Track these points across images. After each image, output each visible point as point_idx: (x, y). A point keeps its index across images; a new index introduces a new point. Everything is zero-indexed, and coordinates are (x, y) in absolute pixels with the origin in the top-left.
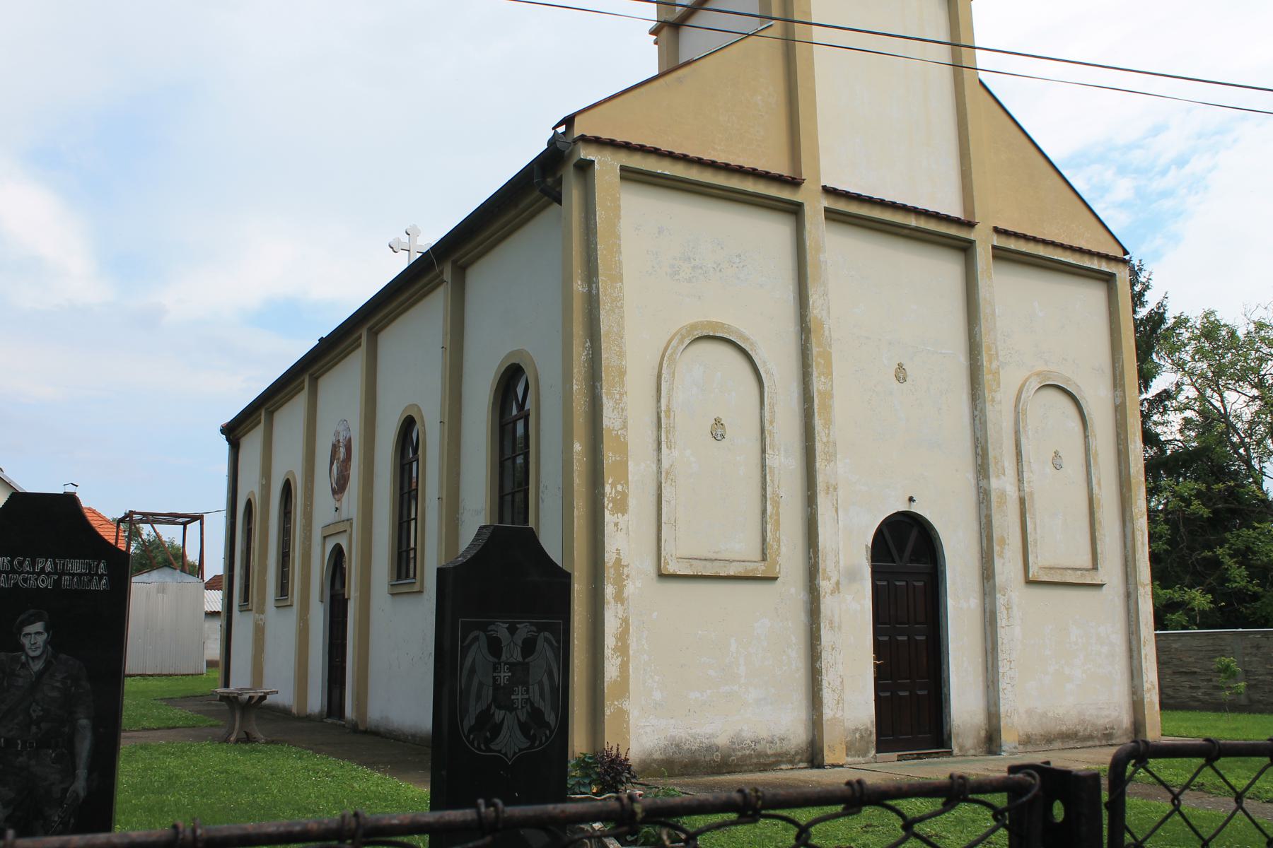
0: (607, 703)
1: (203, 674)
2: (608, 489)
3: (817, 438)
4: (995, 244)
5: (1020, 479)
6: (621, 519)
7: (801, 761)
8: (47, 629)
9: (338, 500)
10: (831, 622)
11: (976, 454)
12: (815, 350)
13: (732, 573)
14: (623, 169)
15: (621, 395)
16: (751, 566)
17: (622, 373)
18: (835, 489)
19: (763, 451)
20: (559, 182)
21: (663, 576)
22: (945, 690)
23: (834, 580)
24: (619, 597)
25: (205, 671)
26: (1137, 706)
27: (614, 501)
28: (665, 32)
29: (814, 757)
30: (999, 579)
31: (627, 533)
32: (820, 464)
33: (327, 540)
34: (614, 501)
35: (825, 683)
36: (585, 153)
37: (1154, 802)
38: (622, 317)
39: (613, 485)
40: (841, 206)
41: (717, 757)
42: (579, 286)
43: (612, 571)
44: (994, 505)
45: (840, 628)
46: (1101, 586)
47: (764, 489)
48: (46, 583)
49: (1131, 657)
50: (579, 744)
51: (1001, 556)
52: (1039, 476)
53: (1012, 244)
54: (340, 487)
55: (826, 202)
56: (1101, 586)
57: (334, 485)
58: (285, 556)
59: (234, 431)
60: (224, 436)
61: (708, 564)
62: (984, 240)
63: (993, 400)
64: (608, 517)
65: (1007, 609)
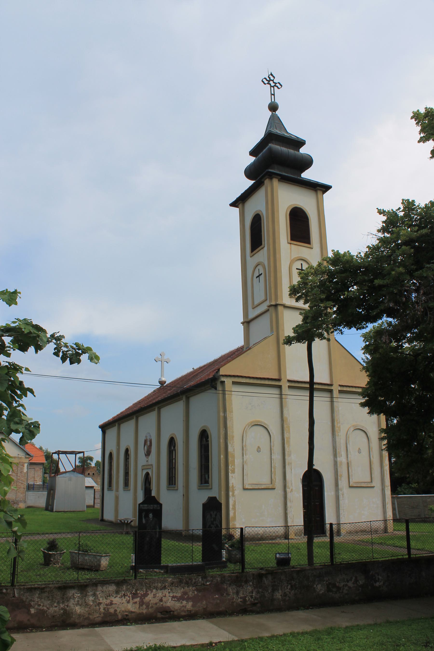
0: (230, 522)
1: (85, 511)
2: (230, 467)
3: (286, 450)
4: (339, 389)
5: (347, 457)
6: (233, 475)
7: (282, 538)
8: (152, 514)
9: (147, 458)
10: (290, 500)
11: (334, 451)
12: (285, 426)
13: (263, 488)
14: (232, 382)
15: (233, 443)
16: (268, 486)
17: (233, 437)
18: (291, 464)
19: (271, 454)
20: (216, 384)
21: (245, 489)
22: (324, 518)
23: (291, 489)
24: (233, 495)
25: (86, 510)
26: (385, 521)
27: (232, 470)
28: (245, 324)
29: (286, 536)
30: (340, 487)
31: (235, 479)
32: (286, 457)
33: (143, 470)
34: (232, 470)
35: (288, 517)
36: (223, 379)
37: (367, 547)
38: (233, 422)
39: (231, 466)
40: (293, 384)
41: (259, 536)
42: (222, 414)
43: (231, 488)
44: (338, 465)
45: (292, 502)
46: (374, 487)
47: (271, 465)
48: (152, 508)
49: (384, 508)
50: (224, 532)
51: (341, 480)
52: (353, 455)
53: (345, 389)
54: (148, 454)
55: (288, 384)
56: (374, 487)
57: (146, 453)
58: (127, 474)
59: (104, 428)
60: (101, 429)
61: (256, 486)
62: (336, 389)
63: (338, 435)
64: (230, 475)
65: (342, 495)
